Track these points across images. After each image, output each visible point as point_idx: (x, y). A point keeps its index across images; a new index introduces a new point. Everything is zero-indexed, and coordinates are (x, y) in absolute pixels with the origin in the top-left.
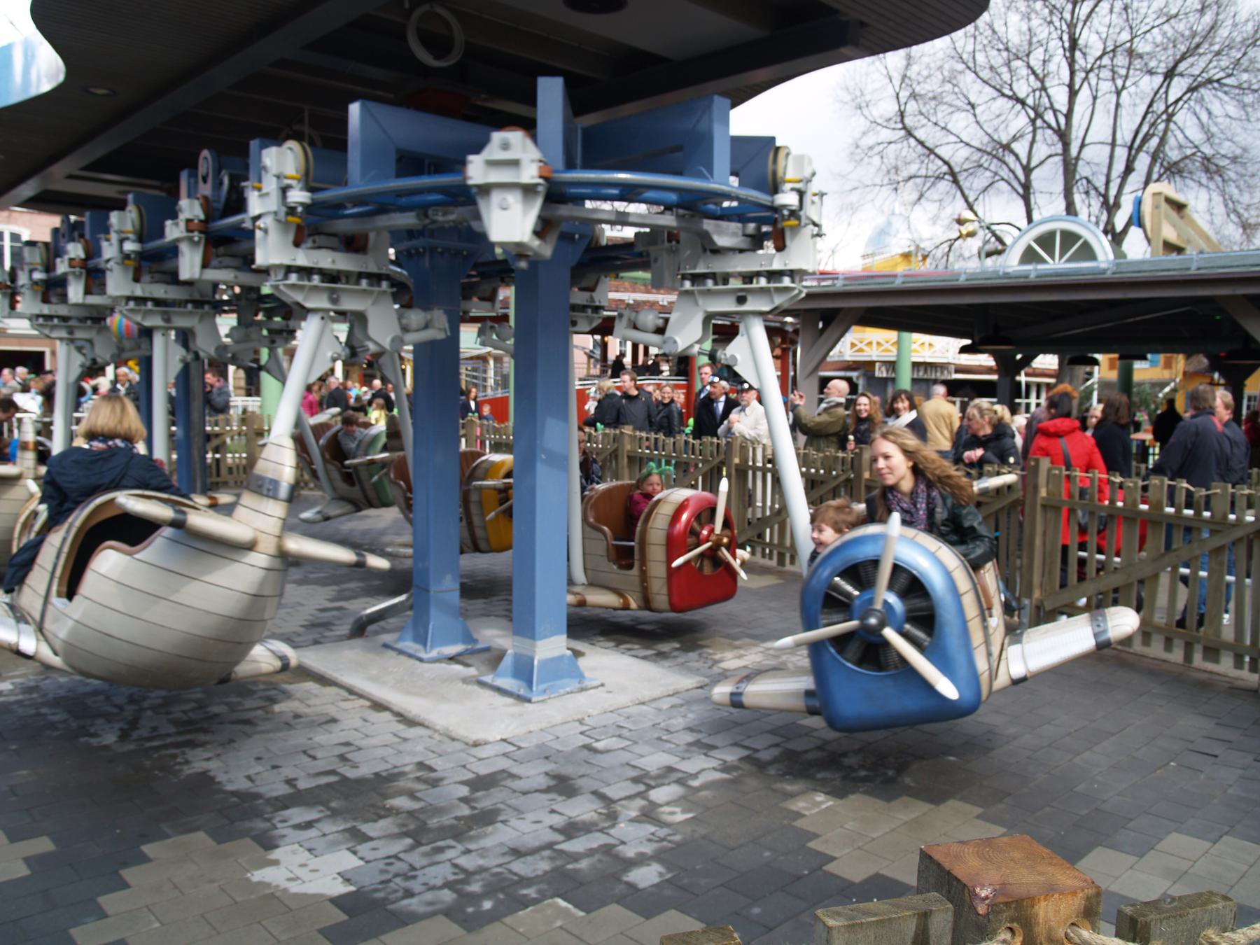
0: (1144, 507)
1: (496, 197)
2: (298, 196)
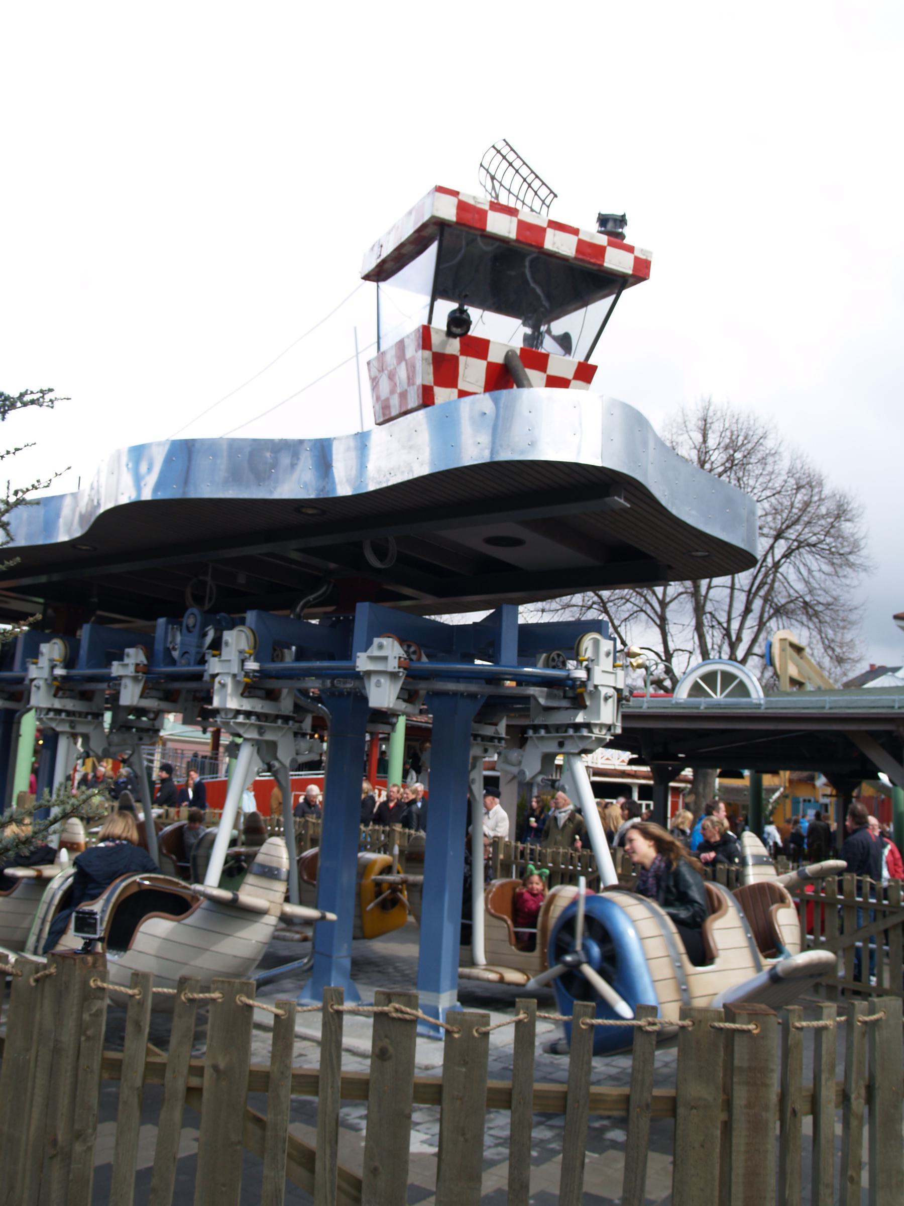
0: (823, 895)
1: (374, 680)
2: (59, 672)
